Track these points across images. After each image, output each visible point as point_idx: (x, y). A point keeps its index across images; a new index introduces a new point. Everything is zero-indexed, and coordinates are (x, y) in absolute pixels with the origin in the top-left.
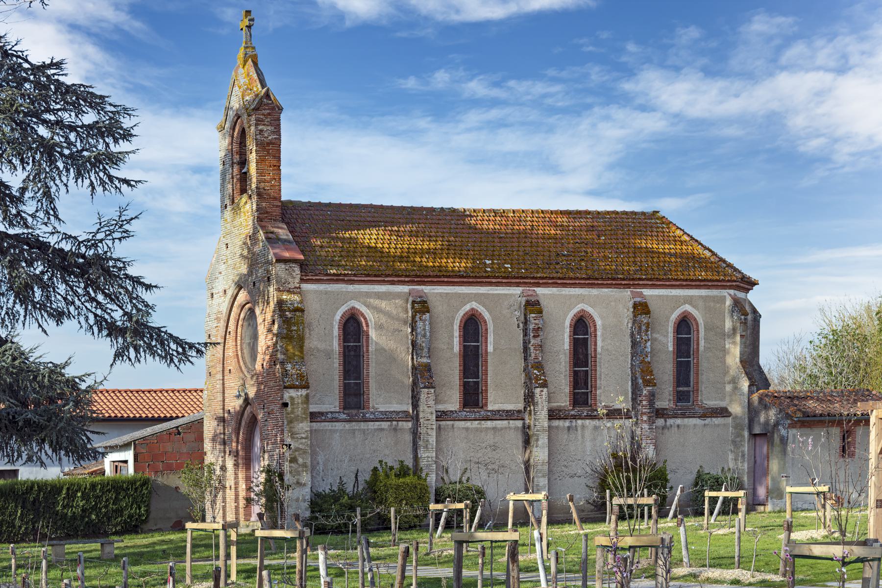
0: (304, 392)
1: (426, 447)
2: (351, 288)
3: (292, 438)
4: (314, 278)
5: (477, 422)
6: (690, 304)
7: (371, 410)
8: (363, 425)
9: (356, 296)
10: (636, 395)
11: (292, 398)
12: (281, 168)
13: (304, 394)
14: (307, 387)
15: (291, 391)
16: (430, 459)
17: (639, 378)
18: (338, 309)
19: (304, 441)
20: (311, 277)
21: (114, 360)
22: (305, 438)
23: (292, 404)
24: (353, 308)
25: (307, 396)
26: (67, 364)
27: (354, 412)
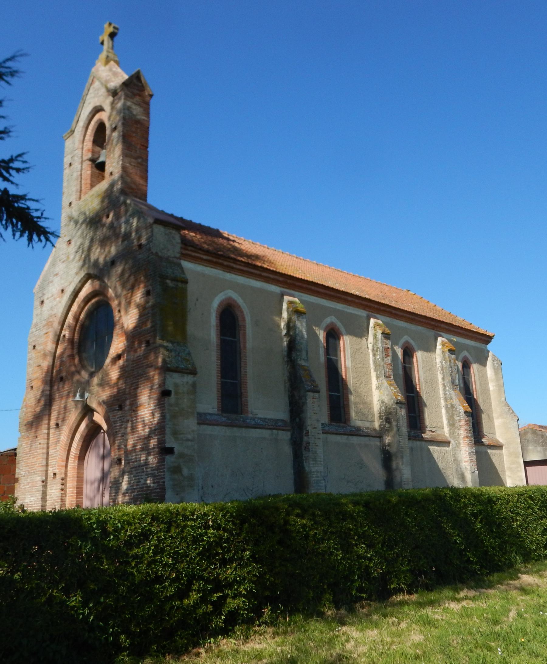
0: (189, 379)
2: (229, 276)
6: (467, 351)
7: (250, 415)
8: (244, 432)
9: (234, 286)
10: (454, 420)
11: (176, 385)
12: (149, 149)
13: (190, 382)
14: (193, 372)
15: (175, 375)
16: (319, 474)
17: (116, 445)
18: (216, 295)
19: (190, 443)
20: (190, 253)
22: (192, 441)
23: (177, 393)
24: (230, 298)
25: (194, 385)
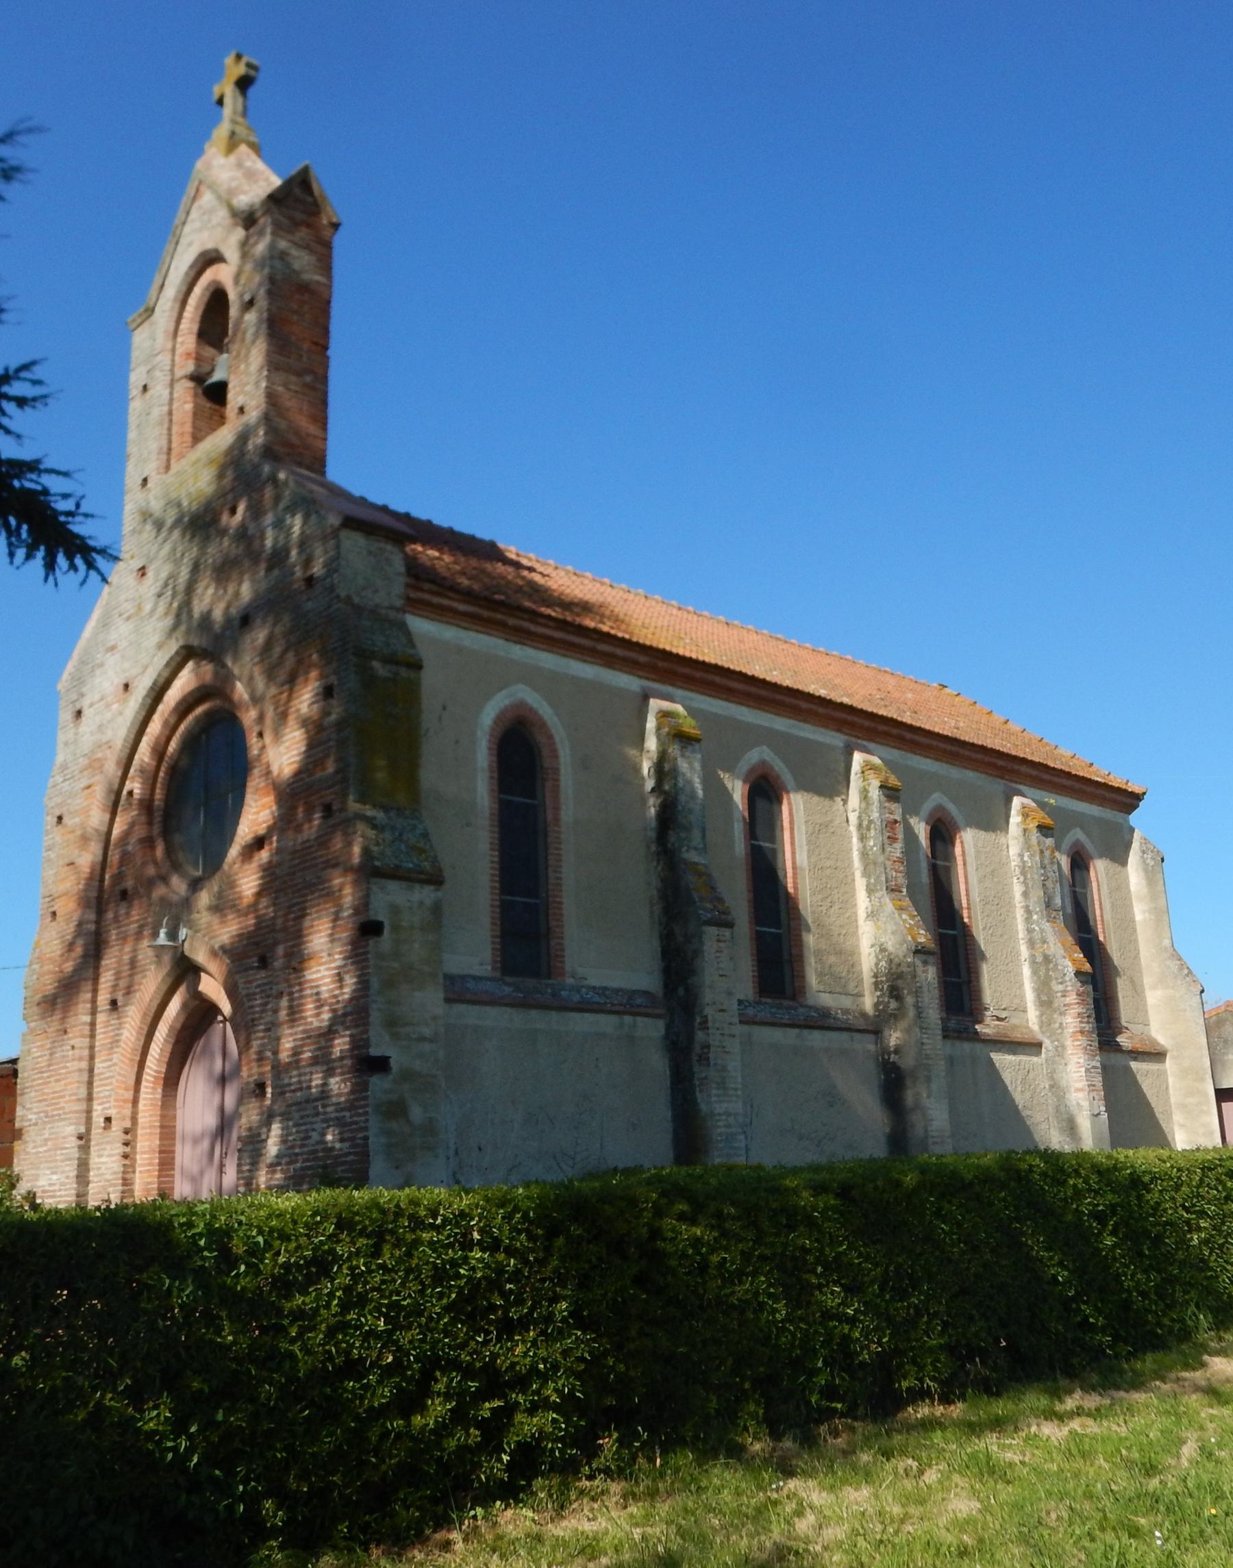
0: (425, 894)
1: (722, 1085)
3: (395, 1036)
4: (436, 600)
5: (794, 1032)
7: (570, 981)
9: (531, 676)
11: (395, 910)
14: (435, 879)
15: (393, 886)
16: (731, 1120)
19: (427, 1047)
20: (427, 596)
21: (76, 480)
22: (431, 1041)
23: (396, 928)
24: (522, 705)
25: (437, 910)
26: (33, 171)
27: (530, 983)
